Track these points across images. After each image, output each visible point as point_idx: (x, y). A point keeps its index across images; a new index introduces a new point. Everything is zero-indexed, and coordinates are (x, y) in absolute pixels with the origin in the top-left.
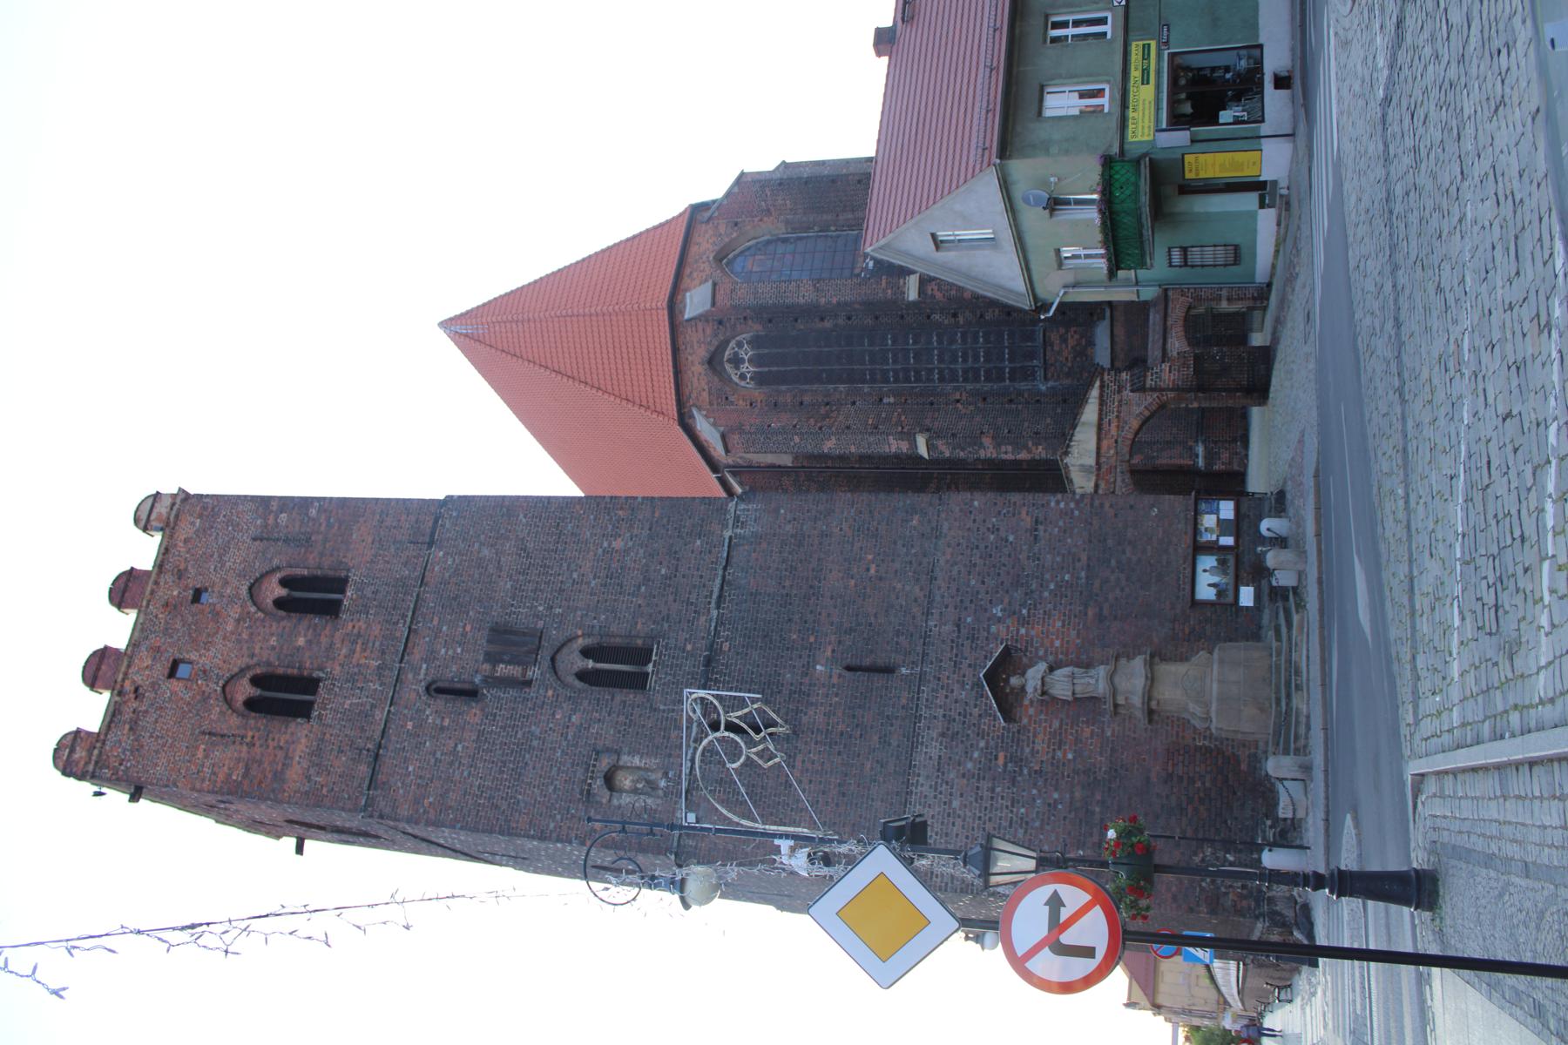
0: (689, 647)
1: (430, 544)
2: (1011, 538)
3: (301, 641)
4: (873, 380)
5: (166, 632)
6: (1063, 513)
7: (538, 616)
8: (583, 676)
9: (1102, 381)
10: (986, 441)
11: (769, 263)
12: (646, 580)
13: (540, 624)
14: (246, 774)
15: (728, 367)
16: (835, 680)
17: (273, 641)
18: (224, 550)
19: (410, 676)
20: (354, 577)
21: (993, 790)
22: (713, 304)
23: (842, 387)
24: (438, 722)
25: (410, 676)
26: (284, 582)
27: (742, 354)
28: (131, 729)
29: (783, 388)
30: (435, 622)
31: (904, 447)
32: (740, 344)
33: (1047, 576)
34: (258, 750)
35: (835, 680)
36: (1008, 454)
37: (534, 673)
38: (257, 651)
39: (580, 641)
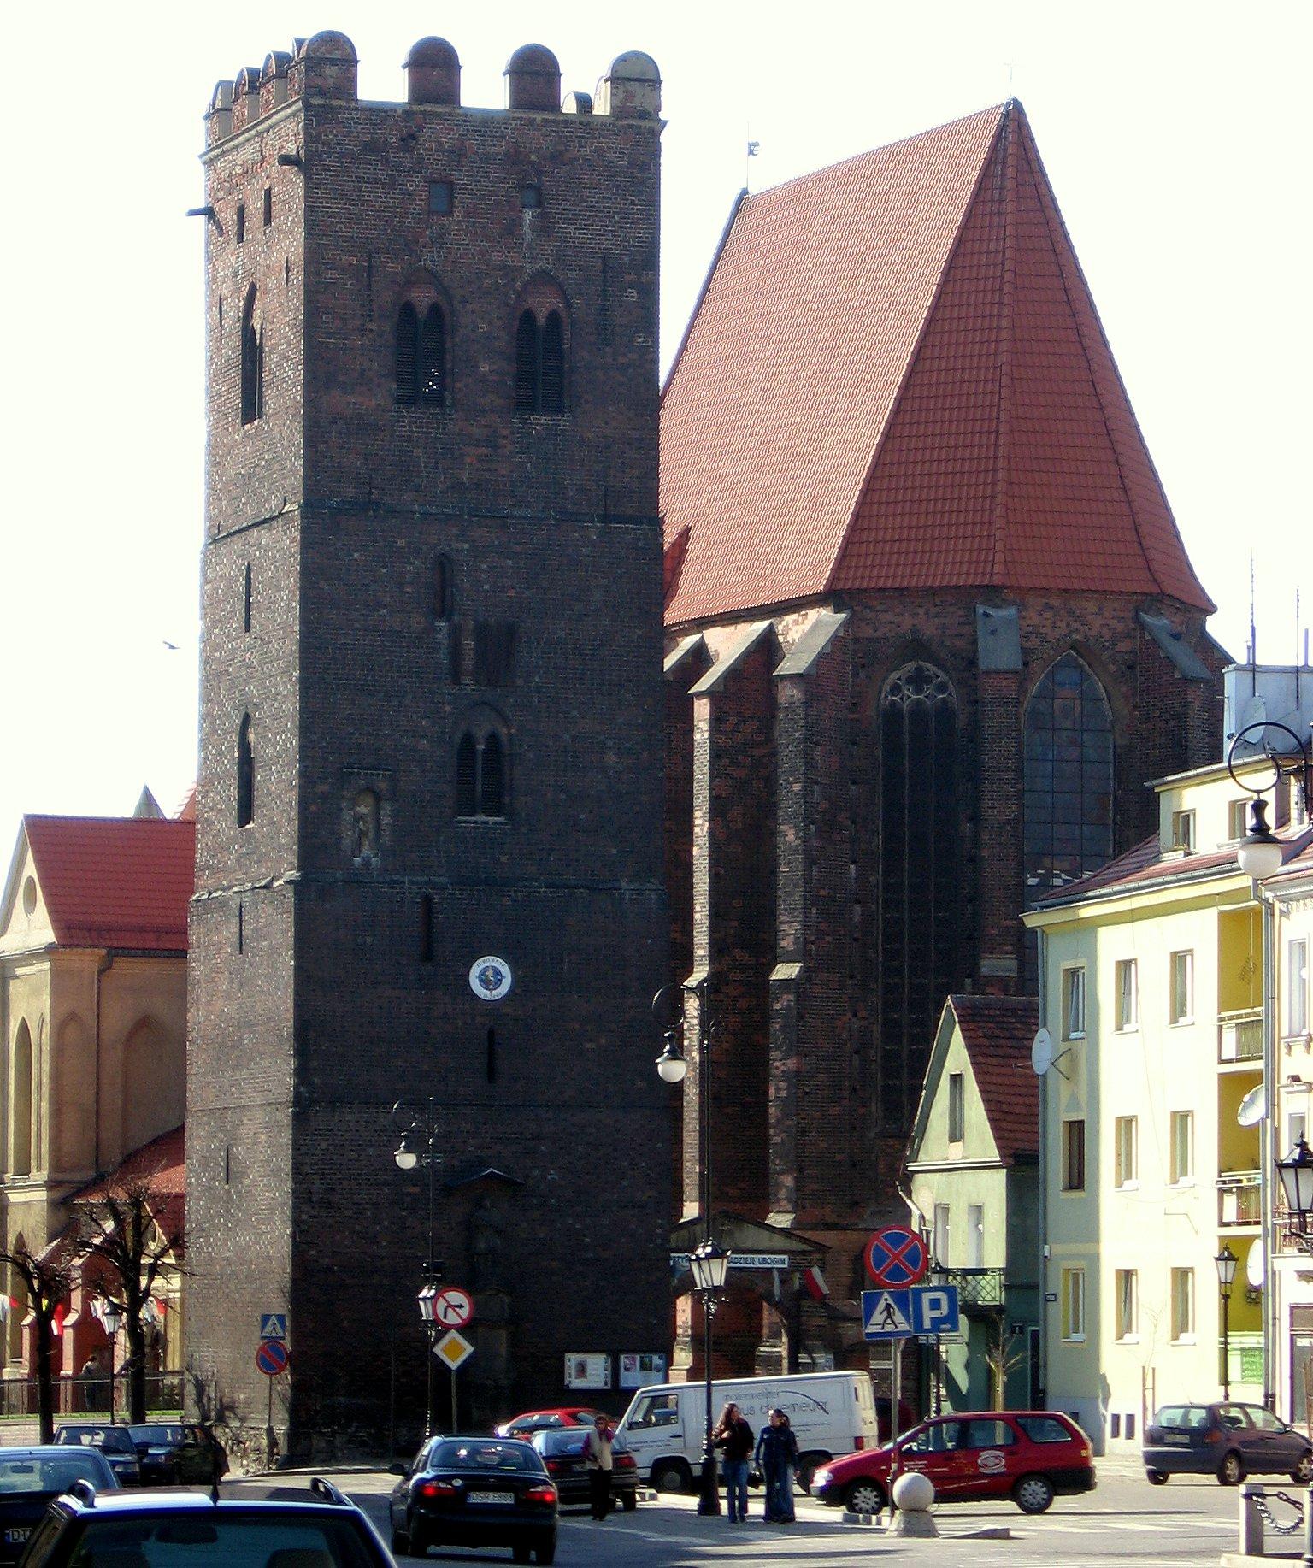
0: (504, 859)
1: (606, 518)
2: (625, 1183)
3: (484, 368)
4: (887, 887)
8: (468, 739)
9: (810, 1252)
10: (791, 1063)
11: (1068, 724)
13: (520, 682)
15: (911, 665)
16: (479, 1019)
17: (483, 327)
19: (455, 531)
20: (564, 422)
21: (386, 1184)
22: (987, 673)
23: (879, 840)
24: (408, 578)
25: (455, 531)
26: (553, 316)
27: (929, 690)
28: (366, 144)
29: (879, 753)
30: (517, 549)
31: (786, 943)
32: (942, 688)
33: (588, 1221)
35: (479, 1019)
36: (776, 1090)
38: (470, 307)
39: (505, 731)
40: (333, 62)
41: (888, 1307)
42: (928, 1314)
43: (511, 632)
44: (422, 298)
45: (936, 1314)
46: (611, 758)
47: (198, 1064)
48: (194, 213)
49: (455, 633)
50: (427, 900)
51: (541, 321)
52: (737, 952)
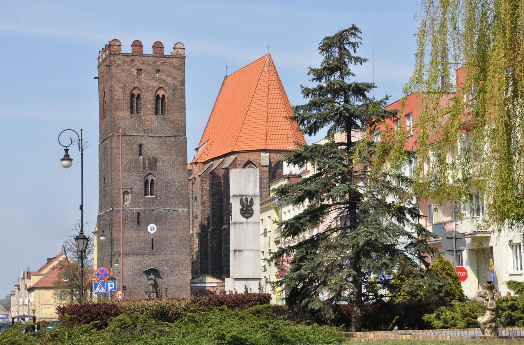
1: (175, 136)
5: (148, 64)
6: (186, 279)
7: (159, 168)
8: (147, 180)
12: (169, 192)
14: (117, 100)
17: (149, 98)
18: (170, 76)
34: (123, 101)
37: (147, 169)
40: (116, 45)
41: (100, 286)
42: (110, 288)
43: (156, 160)
44: (136, 92)
45: (111, 288)
46: (177, 184)
47: (232, 254)
48: (95, 78)
49: (144, 159)
50: (139, 213)
51: (161, 97)
52: (218, 224)
